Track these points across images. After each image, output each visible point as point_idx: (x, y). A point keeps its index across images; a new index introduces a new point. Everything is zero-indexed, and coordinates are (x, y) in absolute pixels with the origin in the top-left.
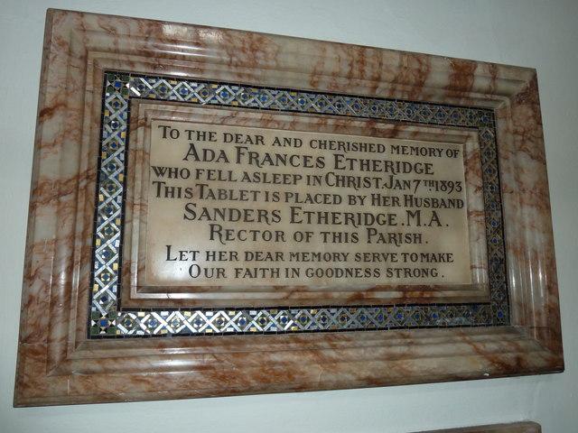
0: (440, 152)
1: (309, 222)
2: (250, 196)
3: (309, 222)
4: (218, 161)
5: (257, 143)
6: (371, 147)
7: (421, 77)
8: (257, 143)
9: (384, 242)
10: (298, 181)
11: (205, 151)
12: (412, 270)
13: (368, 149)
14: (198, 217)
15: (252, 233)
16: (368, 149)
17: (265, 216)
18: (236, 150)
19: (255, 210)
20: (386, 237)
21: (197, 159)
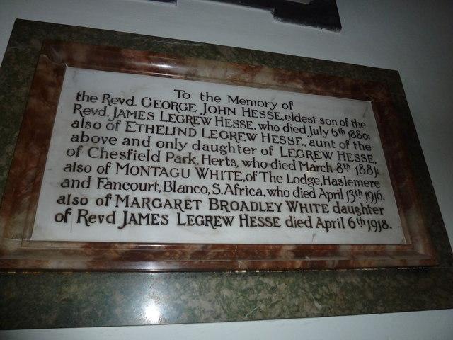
0: (279, 207)
1: (140, 131)
2: (193, 205)
3: (140, 131)
4: (164, 208)
5: (143, 206)
6: (140, 115)
7: (228, 306)
8: (143, 206)
9: (171, 207)
10: (112, 213)
11: (251, 203)
12: (229, 203)
13: (224, 124)
14: (163, 206)
15: (195, 202)
16: (224, 124)
17: (147, 204)
18: (78, 211)
19: (71, 204)
20: (140, 202)
21: (139, 206)
